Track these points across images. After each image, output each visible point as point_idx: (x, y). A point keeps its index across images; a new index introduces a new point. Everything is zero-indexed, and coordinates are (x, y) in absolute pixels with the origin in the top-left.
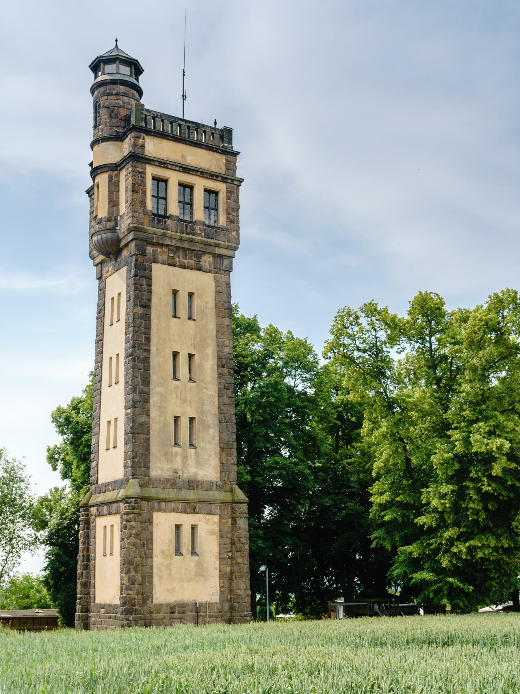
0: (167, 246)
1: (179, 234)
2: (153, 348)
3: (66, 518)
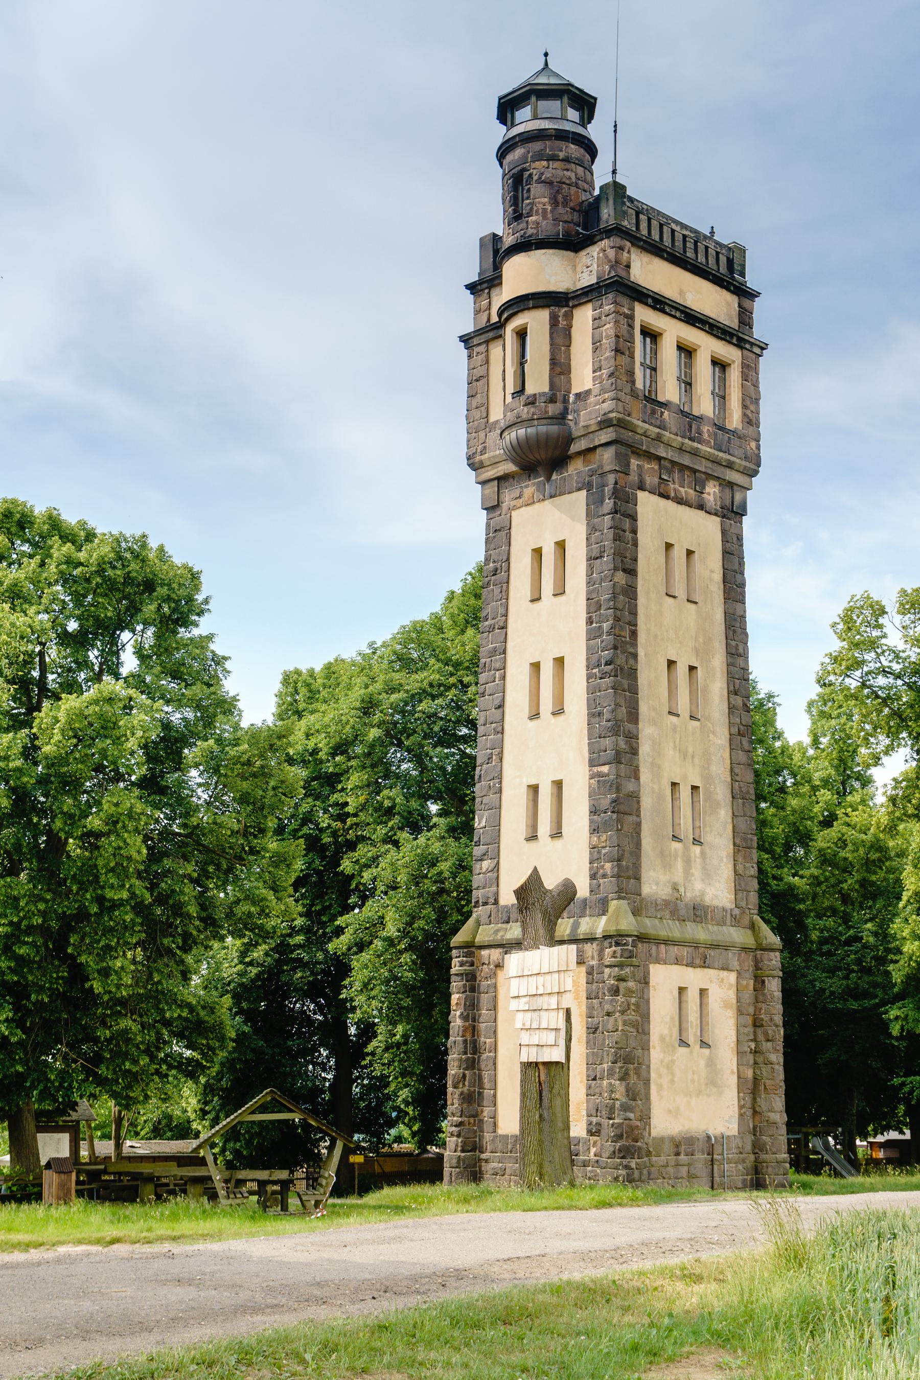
0: (659, 459)
1: (679, 439)
2: (641, 652)
3: (250, 964)
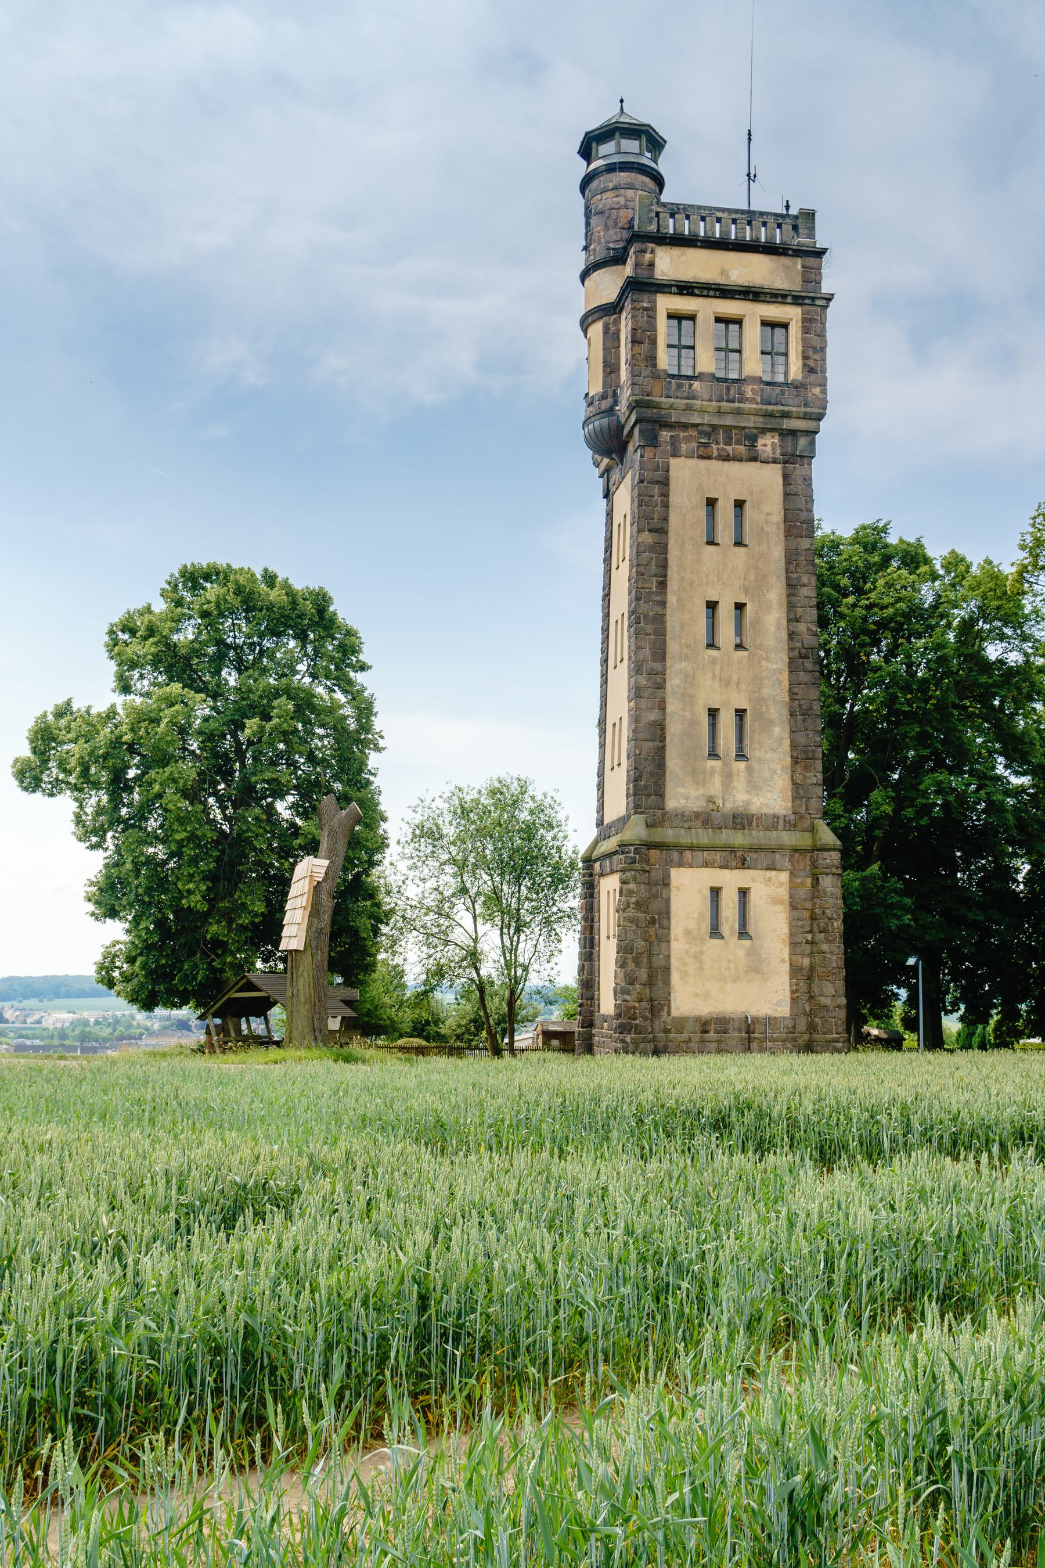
1: (714, 403)
